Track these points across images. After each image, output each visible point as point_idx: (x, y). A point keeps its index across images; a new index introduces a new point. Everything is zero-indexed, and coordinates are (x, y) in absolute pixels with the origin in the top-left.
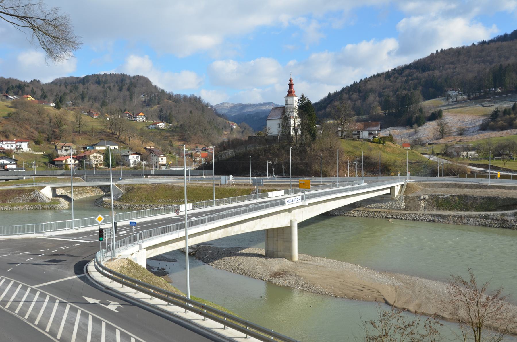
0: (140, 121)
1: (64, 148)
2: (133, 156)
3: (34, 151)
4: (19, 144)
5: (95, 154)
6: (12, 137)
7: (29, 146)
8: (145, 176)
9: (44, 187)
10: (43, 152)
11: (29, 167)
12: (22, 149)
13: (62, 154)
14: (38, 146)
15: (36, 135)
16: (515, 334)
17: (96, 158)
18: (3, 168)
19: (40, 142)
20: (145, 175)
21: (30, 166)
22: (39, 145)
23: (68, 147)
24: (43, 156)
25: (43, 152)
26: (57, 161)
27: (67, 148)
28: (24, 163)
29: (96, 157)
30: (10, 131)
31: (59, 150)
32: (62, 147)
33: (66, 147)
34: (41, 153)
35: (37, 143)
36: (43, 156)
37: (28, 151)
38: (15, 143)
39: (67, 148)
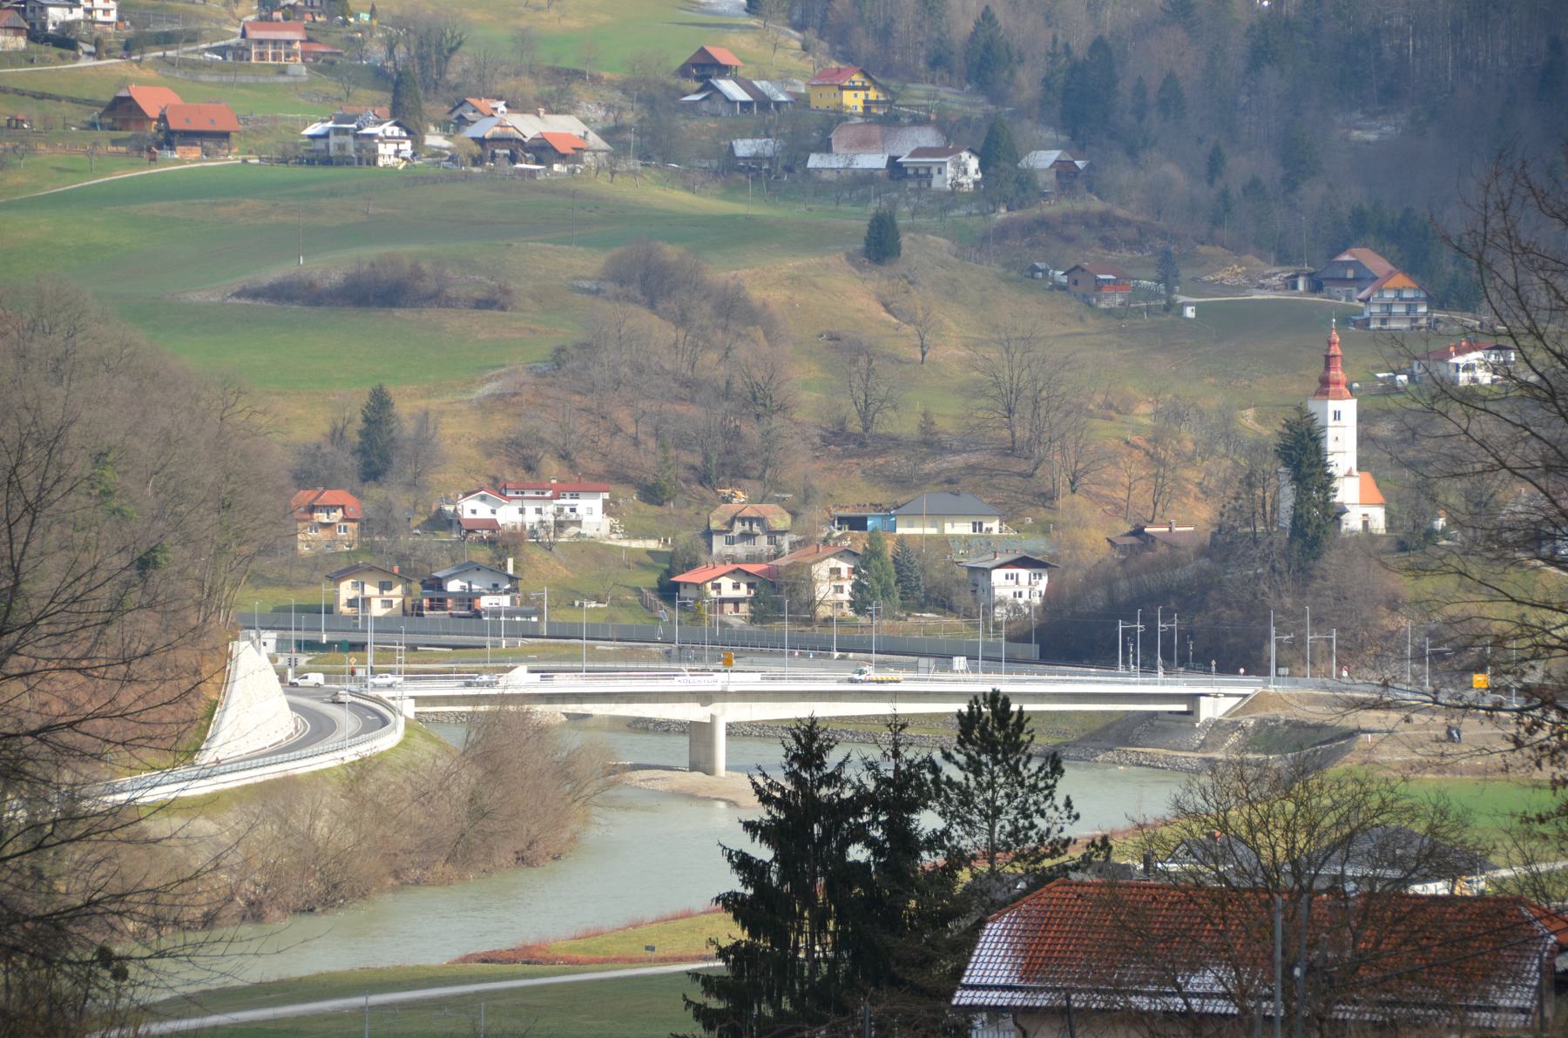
0: (1394, 325)
1: (738, 528)
2: (1014, 571)
3: (632, 533)
4: (567, 502)
5: (834, 563)
6: (552, 468)
7: (608, 509)
8: (836, 655)
9: (512, 669)
10: (666, 541)
11: (573, 605)
12: (578, 523)
13: (730, 550)
14: (655, 509)
15: (647, 461)
16: (1290, 1036)
17: (839, 578)
18: (469, 608)
19: (663, 490)
20: (838, 650)
21: (577, 603)
22: (660, 504)
23: (755, 525)
24: (649, 560)
25: (666, 541)
26: (686, 584)
27: (751, 525)
28: (362, 646)
29: (835, 571)
30: (542, 441)
31: (715, 538)
32: (731, 524)
33: (747, 524)
34: (652, 544)
35: (653, 494)
36: (649, 560)
37: (605, 529)
38: (551, 498)
39: (751, 525)
